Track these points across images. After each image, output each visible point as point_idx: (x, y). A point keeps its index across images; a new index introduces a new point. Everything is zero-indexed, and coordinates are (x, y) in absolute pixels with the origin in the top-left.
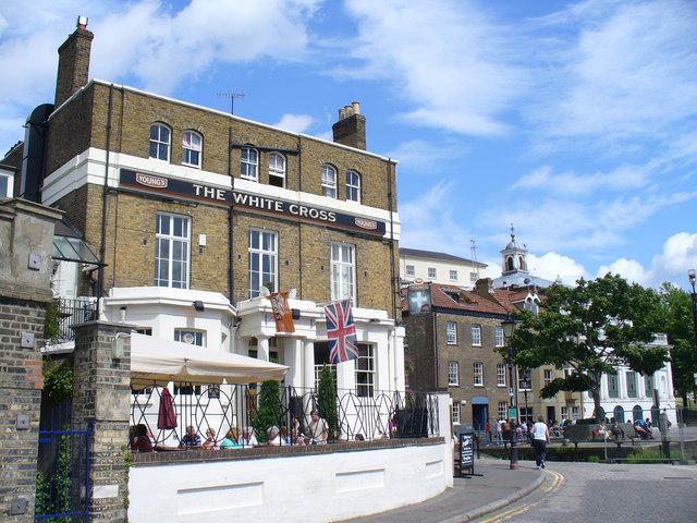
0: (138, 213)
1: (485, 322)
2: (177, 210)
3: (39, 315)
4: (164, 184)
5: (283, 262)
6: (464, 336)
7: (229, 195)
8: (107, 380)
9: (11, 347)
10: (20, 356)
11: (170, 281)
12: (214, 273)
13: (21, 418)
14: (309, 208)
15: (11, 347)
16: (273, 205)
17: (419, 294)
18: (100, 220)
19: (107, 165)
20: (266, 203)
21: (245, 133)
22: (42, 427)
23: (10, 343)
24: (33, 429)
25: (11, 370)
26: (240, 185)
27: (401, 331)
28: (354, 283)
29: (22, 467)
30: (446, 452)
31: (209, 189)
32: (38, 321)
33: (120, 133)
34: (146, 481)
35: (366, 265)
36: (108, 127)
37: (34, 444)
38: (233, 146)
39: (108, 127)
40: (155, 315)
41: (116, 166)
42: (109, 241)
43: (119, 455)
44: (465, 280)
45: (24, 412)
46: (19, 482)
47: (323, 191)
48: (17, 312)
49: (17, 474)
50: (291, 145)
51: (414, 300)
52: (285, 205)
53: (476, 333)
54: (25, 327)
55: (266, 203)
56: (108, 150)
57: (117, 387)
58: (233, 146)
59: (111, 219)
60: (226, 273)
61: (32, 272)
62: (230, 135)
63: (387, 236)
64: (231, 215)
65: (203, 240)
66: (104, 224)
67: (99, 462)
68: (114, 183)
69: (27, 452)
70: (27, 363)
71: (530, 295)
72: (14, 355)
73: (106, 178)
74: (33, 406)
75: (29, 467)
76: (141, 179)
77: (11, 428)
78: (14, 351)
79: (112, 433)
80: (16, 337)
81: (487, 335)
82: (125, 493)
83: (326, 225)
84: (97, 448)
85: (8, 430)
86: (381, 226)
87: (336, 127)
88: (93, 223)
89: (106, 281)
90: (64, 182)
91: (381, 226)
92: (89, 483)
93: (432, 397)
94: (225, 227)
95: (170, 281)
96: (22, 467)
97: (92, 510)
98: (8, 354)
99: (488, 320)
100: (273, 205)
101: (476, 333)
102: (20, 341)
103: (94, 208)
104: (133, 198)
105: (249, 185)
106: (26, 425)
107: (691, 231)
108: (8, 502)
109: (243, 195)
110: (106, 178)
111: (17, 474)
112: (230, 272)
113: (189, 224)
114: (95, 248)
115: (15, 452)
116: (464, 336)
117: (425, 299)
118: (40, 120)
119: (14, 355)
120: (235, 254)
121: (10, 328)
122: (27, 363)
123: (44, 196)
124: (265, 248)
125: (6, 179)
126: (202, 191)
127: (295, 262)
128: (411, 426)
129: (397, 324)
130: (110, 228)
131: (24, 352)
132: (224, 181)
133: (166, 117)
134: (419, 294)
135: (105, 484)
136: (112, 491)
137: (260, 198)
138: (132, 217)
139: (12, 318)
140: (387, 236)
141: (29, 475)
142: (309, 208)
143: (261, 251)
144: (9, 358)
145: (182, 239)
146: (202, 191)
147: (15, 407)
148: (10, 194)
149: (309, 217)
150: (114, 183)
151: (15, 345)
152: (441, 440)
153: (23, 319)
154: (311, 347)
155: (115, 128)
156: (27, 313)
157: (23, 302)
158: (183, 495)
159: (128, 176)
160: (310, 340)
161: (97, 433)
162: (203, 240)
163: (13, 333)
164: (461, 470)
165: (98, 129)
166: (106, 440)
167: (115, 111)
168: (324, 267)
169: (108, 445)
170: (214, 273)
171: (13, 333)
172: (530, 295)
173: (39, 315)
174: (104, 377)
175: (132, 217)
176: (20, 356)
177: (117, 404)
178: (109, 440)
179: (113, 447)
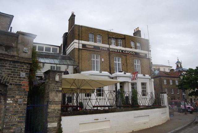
1: (173, 79)
3: (27, 67)
4: (93, 47)
5: (122, 64)
6: (168, 82)
7: (109, 49)
8: (53, 88)
9: (16, 77)
10: (20, 80)
11: (96, 70)
12: (106, 68)
13: (20, 100)
14: (128, 51)
15: (16, 77)
16: (119, 51)
17: (157, 71)
19: (79, 43)
20: (118, 51)
22: (28, 104)
23: (16, 76)
24: (24, 104)
25: (16, 85)
26: (111, 47)
27: (153, 80)
28: (140, 69)
29: (19, 117)
30: (167, 110)
32: (27, 69)
33: (82, 36)
34: (68, 122)
36: (79, 35)
37: (25, 109)
38: (109, 38)
39: (79, 35)
41: (81, 43)
42: (80, 61)
43: (58, 113)
44: (167, 70)
45: (21, 98)
46: (18, 122)
47: (131, 48)
48: (19, 66)
49: (17, 120)
50: (123, 37)
51: (155, 72)
52: (122, 51)
53: (171, 81)
54: (22, 71)
55: (118, 51)
56: (79, 40)
57: (57, 91)
58: (109, 38)
59: (80, 56)
60: (109, 67)
61: (25, 53)
62: (108, 35)
63: (148, 57)
64: (109, 55)
65: (103, 60)
66: (79, 57)
67: (50, 115)
68: (81, 47)
69: (22, 112)
70: (23, 83)
71: (183, 72)
72: (17, 80)
73: (79, 46)
74: (25, 97)
75: (22, 117)
76: (88, 46)
77: (16, 104)
78: (18, 79)
79: (55, 106)
80: (18, 74)
81: (174, 82)
82: (60, 125)
83: (132, 55)
84: (49, 110)
85: (15, 105)
86: (146, 55)
87: (134, 34)
88: (76, 57)
89: (80, 70)
90: (69, 50)
91: (146, 55)
92: (47, 122)
93: (162, 94)
94: (108, 57)
95: (96, 70)
96: (19, 117)
97: (48, 131)
98: (15, 79)
99: (174, 78)
100: (119, 51)
101: (171, 81)
102: (20, 75)
103: (76, 53)
104: (85, 51)
105: (113, 46)
106: (22, 103)
108: (14, 129)
109: (112, 49)
110: (79, 46)
111: (17, 120)
112: (110, 67)
114: (77, 63)
115: (17, 112)
116: (168, 82)
117: (158, 72)
118: (66, 36)
119: (17, 80)
120: (111, 63)
121: (16, 71)
122: (23, 83)
123: (67, 52)
124: (118, 61)
125: (57, 49)
126: (102, 48)
127: (125, 64)
128: (157, 104)
129: (151, 78)
130: (80, 58)
131: (21, 79)
132: (107, 46)
133: (92, 32)
134: (157, 71)
135: (52, 122)
136: (55, 125)
139: (17, 68)
140: (148, 57)
141: (23, 119)
142: (128, 51)
143: (117, 62)
144: (16, 81)
146: (102, 48)
147: (17, 97)
148: (58, 52)
149: (128, 54)
150: (81, 47)
151: (18, 76)
152: (165, 107)
153: (21, 68)
154: (130, 84)
155: (80, 35)
156: (23, 66)
157: (21, 63)
158: (82, 125)
159: (84, 46)
160: (129, 82)
161: (49, 105)
162: (103, 60)
163: (17, 73)
164: (171, 114)
165: (77, 35)
166: (53, 108)
168: (133, 65)
169: (54, 109)
170: (106, 68)
171: (17, 73)
172: (183, 72)
173: (27, 67)
174: (52, 87)
176: (20, 80)
177: (57, 96)
178: (54, 107)
179: (55, 110)
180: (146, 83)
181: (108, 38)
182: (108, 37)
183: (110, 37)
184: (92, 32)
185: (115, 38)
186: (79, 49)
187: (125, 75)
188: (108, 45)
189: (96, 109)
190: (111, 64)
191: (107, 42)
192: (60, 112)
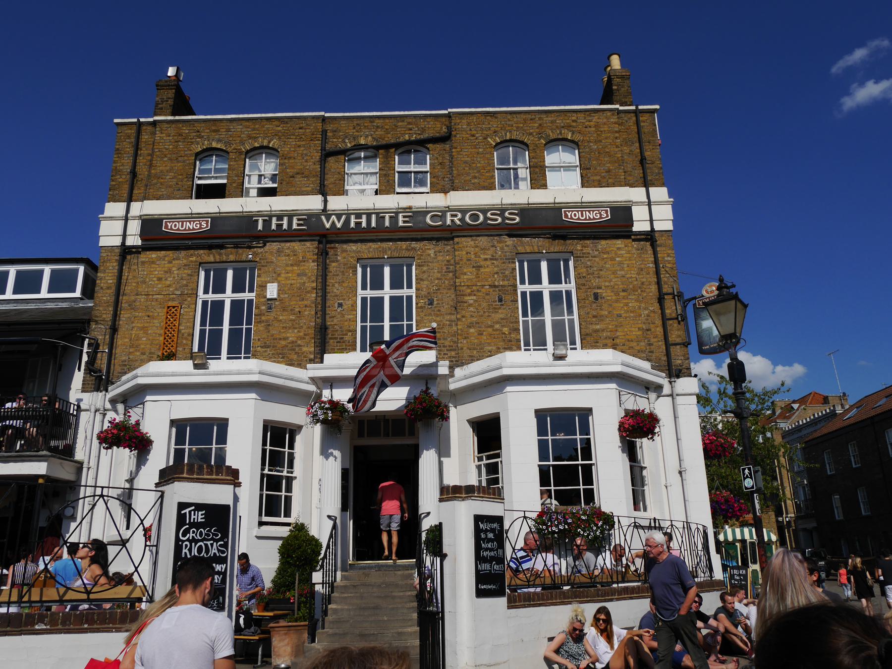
0: (169, 271)
2: (232, 258)
12: (292, 335)
18: (112, 291)
19: (649, 204)
20: (380, 219)
21: (351, 132)
31: (369, 216)
35: (595, 282)
36: (134, 174)
40: (501, 390)
56: (324, 194)
68: (134, 240)
73: (651, 221)
107: (888, 79)
109: (339, 217)
110: (651, 221)
113: (571, 263)
126: (267, 223)
132: (312, 203)
133: (219, 141)
137: (369, 216)
138: (160, 279)
145: (370, 293)
146: (267, 223)
150: (134, 240)
159: (150, 225)
167: (144, 151)
170: (292, 335)
175: (160, 279)
180: (589, 411)
181: (317, 156)
182: (323, 149)
183: (341, 146)
184: (214, 145)
185: (377, 148)
186: (125, 251)
187: (200, 377)
188: (319, 198)
189: (6, 611)
190: (333, 309)
191: (314, 182)
192: (883, 612)
